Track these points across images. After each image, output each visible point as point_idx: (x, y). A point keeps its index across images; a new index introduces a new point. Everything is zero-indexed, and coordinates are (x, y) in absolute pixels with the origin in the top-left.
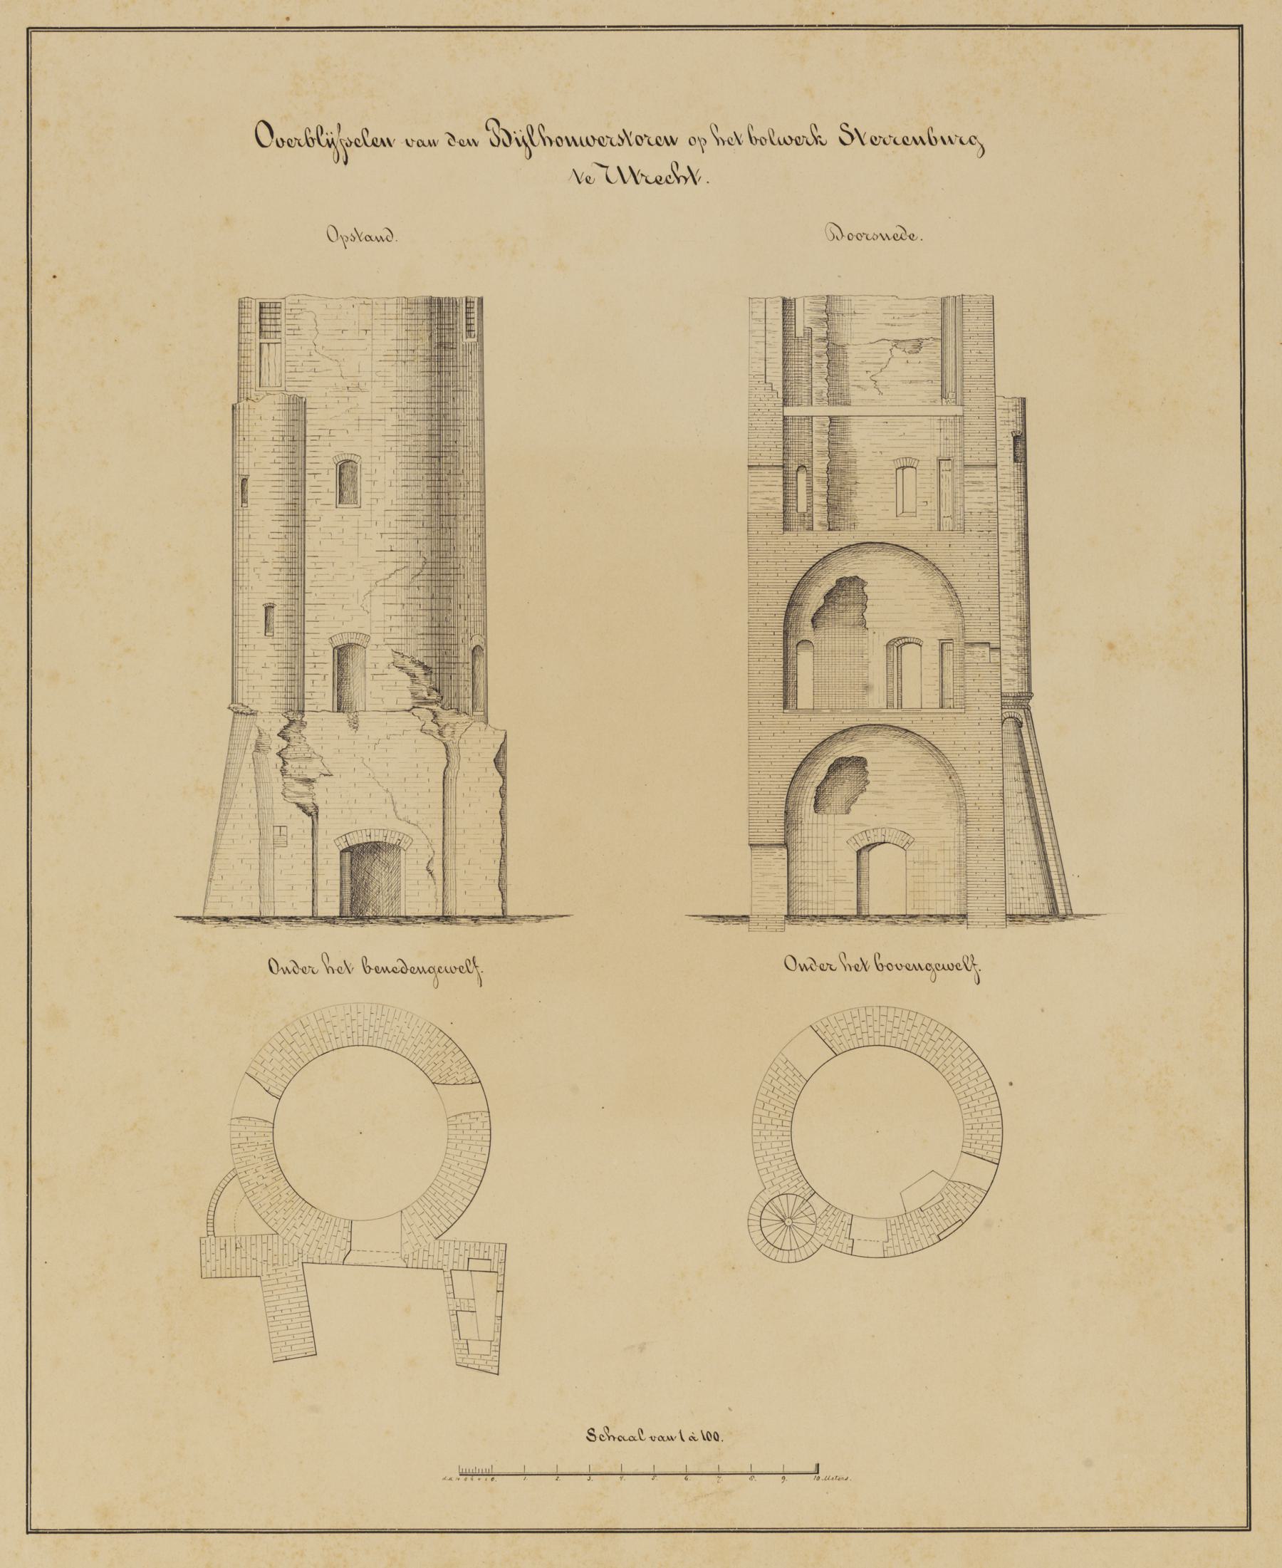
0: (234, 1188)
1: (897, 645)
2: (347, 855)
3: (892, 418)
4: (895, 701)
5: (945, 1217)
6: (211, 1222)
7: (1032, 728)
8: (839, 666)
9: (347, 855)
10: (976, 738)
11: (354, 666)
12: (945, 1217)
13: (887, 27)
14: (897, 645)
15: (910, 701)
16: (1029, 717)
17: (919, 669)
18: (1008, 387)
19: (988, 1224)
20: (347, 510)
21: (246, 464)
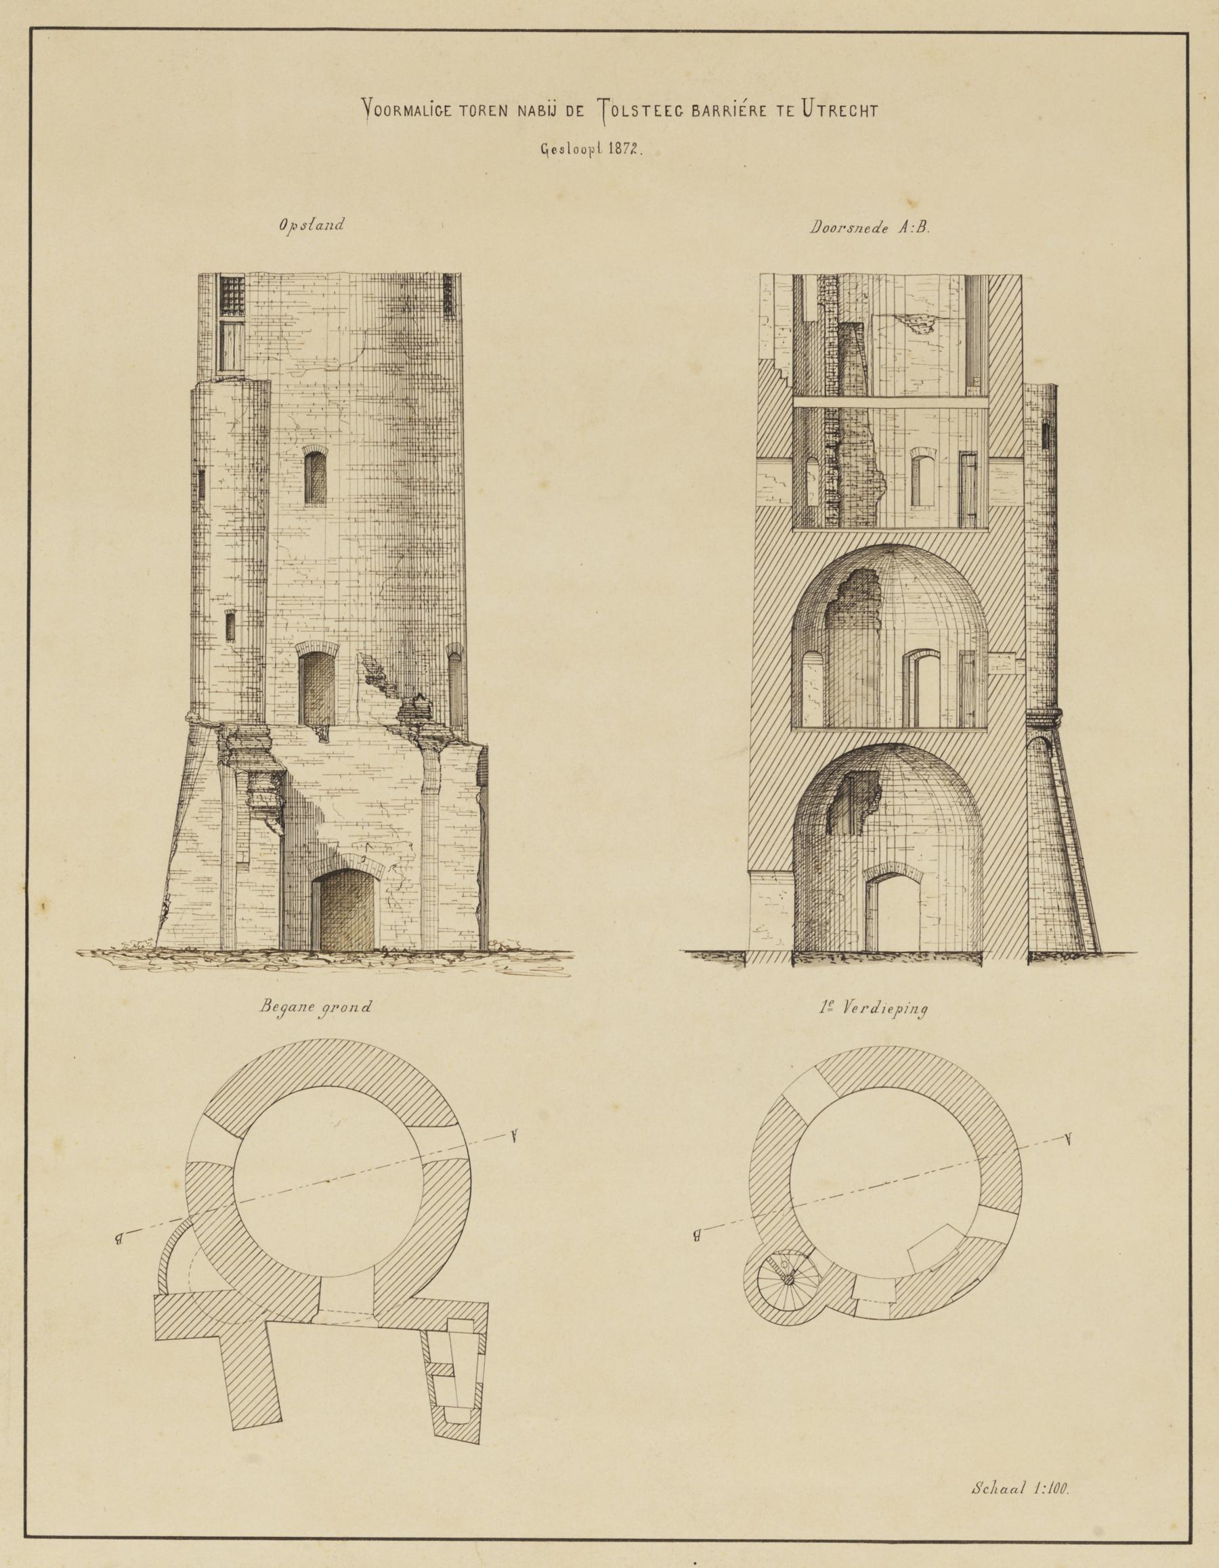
0: (189, 1241)
1: (913, 659)
2: (309, 460)
3: (915, 401)
4: (912, 723)
5: (941, 1286)
6: (164, 1274)
7: (1059, 749)
8: (864, 682)
9: (309, 460)
10: (999, 757)
11: (380, 100)
12: (941, 1286)
13: (26, 1242)
14: (913, 659)
15: (928, 717)
16: (1057, 740)
17: (937, 689)
18: (1037, 377)
19: (506, 971)
20: (317, 510)
21: (206, 458)
